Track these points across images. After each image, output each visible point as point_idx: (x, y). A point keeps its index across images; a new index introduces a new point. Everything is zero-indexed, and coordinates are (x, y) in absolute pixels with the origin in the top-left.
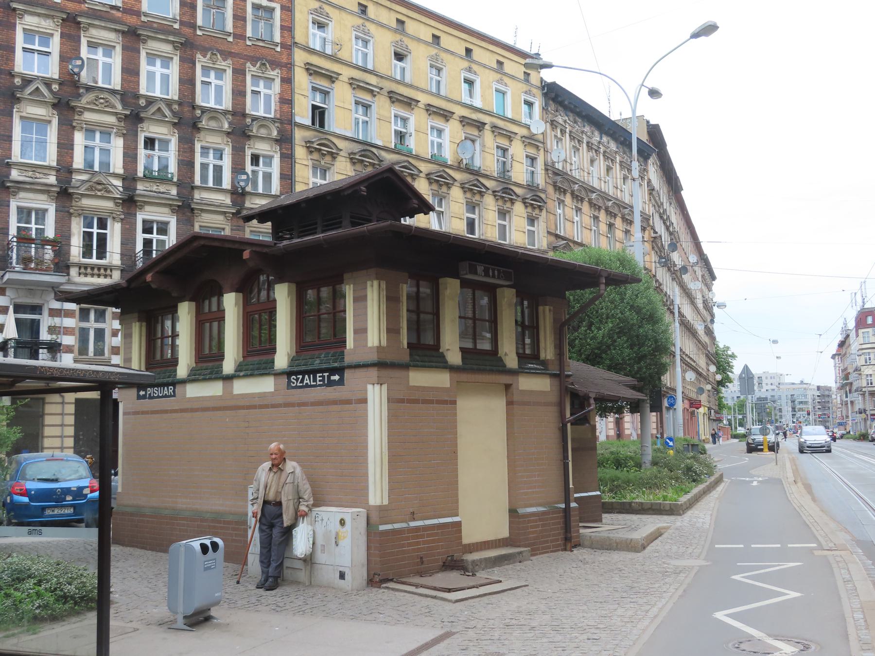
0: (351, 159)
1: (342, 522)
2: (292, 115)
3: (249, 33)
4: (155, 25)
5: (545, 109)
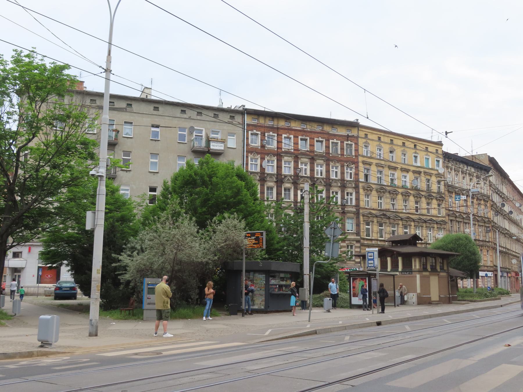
0: (377, 191)
1: (413, 295)
2: (358, 179)
3: (345, 154)
4: (318, 155)
5: (444, 162)
